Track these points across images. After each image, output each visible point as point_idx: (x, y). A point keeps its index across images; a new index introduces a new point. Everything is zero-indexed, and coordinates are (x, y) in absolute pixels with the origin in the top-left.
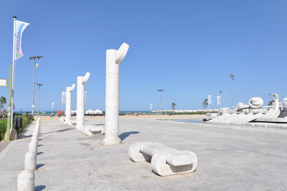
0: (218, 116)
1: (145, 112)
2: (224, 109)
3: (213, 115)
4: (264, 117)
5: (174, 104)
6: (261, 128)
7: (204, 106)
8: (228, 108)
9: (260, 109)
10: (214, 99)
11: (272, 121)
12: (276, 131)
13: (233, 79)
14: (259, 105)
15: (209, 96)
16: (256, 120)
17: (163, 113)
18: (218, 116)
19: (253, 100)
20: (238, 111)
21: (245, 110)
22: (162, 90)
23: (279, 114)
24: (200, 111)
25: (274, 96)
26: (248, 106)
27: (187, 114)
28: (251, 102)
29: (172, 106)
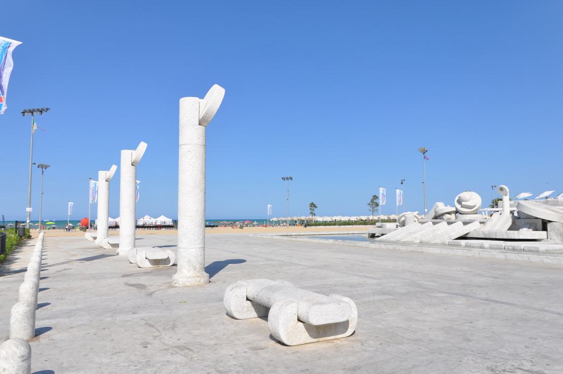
0: (397, 227)
1: (257, 221)
2: (410, 215)
3: (389, 225)
4: (483, 230)
5: (313, 205)
6: (478, 251)
7: (371, 209)
8: (417, 212)
9: (476, 214)
10: (391, 196)
11: (498, 237)
12: (506, 256)
13: (425, 157)
14: (474, 206)
15: (381, 190)
17: (293, 223)
19: (463, 198)
20: (436, 218)
21: (448, 216)
22: (291, 178)
23: (510, 223)
24: (364, 218)
25: (502, 189)
26: (454, 209)
28: (459, 202)
29: (311, 209)
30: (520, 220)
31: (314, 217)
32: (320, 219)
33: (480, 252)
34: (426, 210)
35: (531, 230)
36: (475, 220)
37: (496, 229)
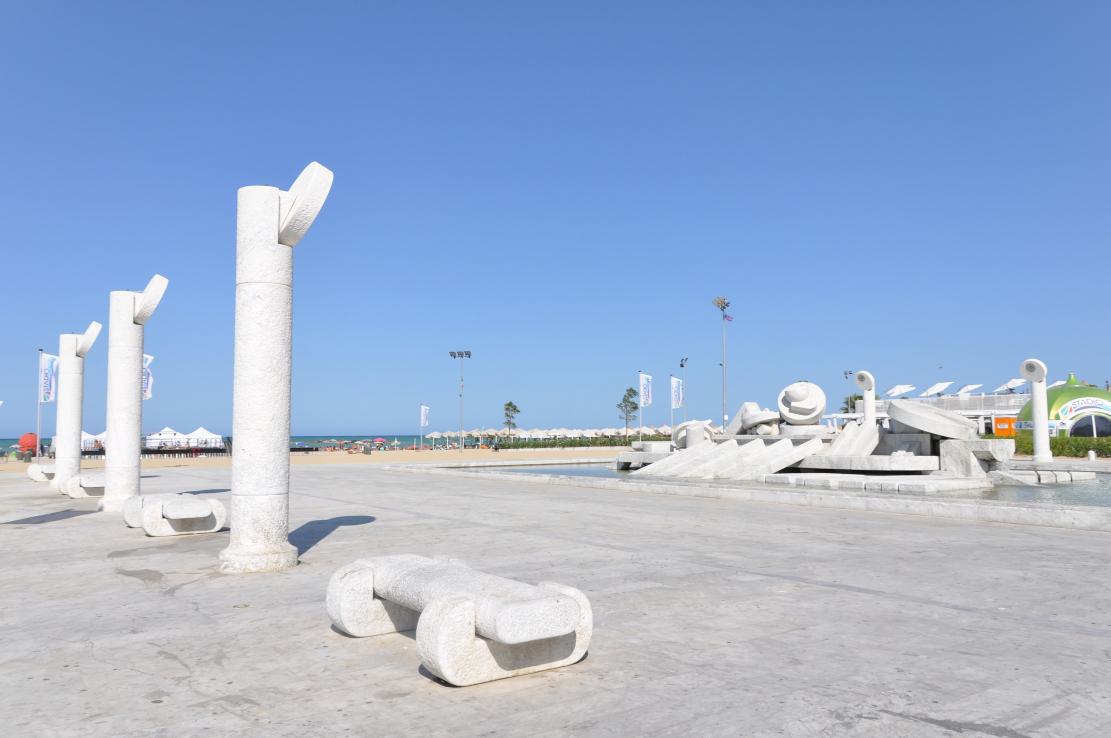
0: (672, 450)
1: (400, 438)
2: (696, 427)
3: (657, 447)
5: (511, 407)
8: (710, 421)
9: (816, 424)
10: (661, 389)
11: (854, 468)
13: (725, 316)
14: (813, 410)
15: (643, 378)
16: (801, 466)
17: (472, 443)
18: (672, 450)
19: (792, 394)
20: (743, 432)
21: (765, 428)
22: (468, 354)
23: (875, 442)
24: (610, 432)
25: (862, 378)
26: (776, 416)
27: (560, 446)
28: (787, 401)
30: (893, 436)
31: (513, 431)
32: (524, 434)
33: (823, 496)
34: (726, 417)
35: (912, 453)
36: (814, 436)
37: (851, 452)
